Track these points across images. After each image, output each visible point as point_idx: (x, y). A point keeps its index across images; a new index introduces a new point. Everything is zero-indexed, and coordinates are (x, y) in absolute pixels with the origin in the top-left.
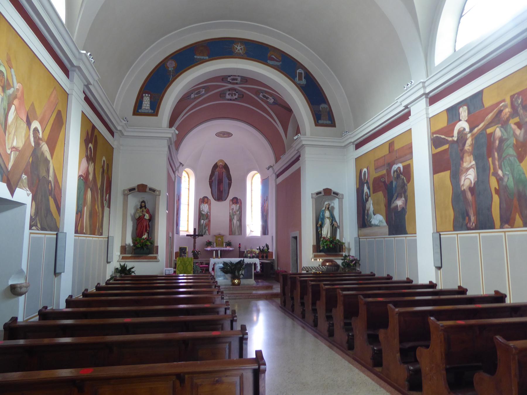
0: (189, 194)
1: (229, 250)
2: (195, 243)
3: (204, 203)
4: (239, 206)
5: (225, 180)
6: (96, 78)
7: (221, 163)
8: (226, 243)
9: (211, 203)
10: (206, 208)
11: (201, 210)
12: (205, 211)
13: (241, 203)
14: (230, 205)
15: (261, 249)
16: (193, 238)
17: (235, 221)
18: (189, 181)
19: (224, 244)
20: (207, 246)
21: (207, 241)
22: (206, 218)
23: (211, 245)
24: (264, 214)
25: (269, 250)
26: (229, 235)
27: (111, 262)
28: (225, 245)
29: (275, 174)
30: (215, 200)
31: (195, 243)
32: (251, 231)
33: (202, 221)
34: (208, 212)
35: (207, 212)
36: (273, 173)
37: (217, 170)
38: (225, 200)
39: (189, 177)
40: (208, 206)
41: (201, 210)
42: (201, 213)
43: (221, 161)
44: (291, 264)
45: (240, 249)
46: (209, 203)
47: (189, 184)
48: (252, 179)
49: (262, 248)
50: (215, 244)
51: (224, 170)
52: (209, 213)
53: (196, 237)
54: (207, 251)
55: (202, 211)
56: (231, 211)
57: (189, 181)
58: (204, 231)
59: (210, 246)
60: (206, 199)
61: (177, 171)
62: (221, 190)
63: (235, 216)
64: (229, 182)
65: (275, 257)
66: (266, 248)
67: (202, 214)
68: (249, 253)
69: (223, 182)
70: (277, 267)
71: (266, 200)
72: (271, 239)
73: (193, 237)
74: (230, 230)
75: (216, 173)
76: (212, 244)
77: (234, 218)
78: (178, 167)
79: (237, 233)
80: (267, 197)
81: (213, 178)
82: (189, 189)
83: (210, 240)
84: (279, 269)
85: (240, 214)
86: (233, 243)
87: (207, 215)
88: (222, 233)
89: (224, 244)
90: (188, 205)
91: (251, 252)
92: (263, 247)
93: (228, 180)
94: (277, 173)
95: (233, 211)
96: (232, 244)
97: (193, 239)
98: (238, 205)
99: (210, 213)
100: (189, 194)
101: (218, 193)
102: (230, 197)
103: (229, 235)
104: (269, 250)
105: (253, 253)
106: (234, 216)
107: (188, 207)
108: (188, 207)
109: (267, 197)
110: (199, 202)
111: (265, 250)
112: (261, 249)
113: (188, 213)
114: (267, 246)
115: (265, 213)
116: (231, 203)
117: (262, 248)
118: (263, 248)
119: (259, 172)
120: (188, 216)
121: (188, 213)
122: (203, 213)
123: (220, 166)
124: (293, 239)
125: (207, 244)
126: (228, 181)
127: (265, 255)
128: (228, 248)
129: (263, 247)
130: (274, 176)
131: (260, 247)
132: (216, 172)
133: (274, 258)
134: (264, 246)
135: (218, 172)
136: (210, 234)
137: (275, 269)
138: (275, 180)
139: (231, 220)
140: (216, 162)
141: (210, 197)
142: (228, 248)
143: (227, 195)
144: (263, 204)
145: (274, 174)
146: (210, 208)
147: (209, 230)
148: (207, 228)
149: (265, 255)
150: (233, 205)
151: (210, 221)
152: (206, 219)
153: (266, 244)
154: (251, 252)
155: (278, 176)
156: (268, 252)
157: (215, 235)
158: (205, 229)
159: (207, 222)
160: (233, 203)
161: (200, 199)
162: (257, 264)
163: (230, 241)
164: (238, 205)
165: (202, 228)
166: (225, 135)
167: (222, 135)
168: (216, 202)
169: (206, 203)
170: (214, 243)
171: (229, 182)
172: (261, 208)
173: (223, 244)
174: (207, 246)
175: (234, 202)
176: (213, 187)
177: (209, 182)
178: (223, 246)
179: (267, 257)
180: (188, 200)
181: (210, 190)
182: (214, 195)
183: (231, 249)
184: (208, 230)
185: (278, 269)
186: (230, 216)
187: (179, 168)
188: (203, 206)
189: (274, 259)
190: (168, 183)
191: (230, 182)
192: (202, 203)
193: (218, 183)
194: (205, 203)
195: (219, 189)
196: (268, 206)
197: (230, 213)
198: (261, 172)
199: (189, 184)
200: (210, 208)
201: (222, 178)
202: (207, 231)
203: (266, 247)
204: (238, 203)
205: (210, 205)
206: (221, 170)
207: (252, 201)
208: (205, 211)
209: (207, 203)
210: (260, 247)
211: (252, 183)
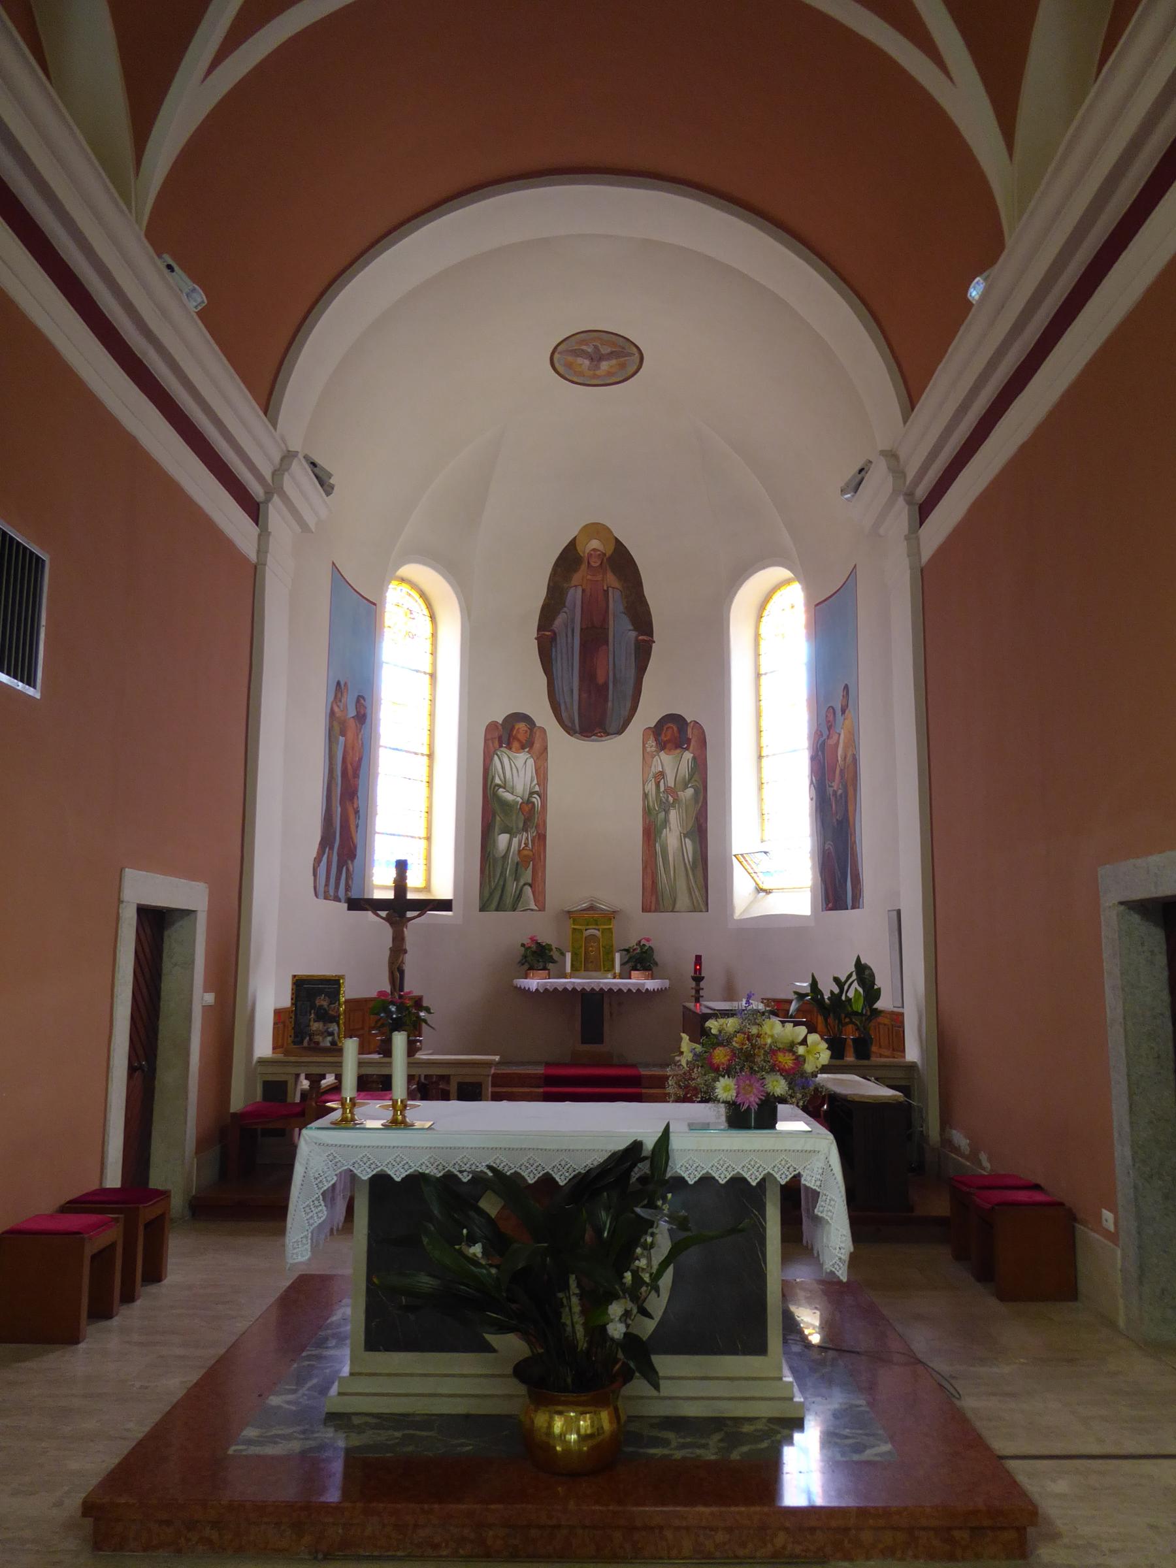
0: (433, 701)
1: (638, 990)
2: (398, 949)
3: (509, 747)
4: (694, 758)
5: (621, 631)
6: (691, 860)
7: (595, 544)
8: (627, 950)
9: (546, 749)
10: (522, 773)
11: (497, 781)
12: (519, 789)
13: (703, 743)
14: (646, 758)
15: (827, 996)
16: (387, 919)
17: (673, 838)
18: (434, 635)
19: (617, 956)
20: (526, 966)
21: (527, 941)
22: (521, 825)
23: (550, 966)
24: (830, 791)
25: (879, 1005)
26: (644, 910)
27: (1116, 902)
28: (622, 964)
29: (909, 495)
30: (570, 730)
31: (398, 949)
32: (759, 890)
33: (503, 839)
34: (531, 793)
35: (526, 796)
36: (895, 492)
37: (577, 578)
38: (620, 732)
39: (433, 617)
40: (531, 762)
41: (497, 781)
42: (495, 795)
43: (596, 529)
44: (1122, 1153)
45: (702, 984)
46: (537, 745)
47: (434, 653)
48: (760, 617)
49: (828, 988)
50: (569, 956)
51: (611, 579)
52: (536, 800)
53: (410, 914)
54: (526, 992)
55: (500, 786)
56: (651, 787)
57: (434, 635)
58: (512, 888)
59: (544, 969)
60: (522, 726)
61: (276, 498)
62: (601, 680)
63: (673, 814)
64: (637, 637)
65: (924, 1051)
66: (854, 990)
67: (505, 805)
68: (729, 1072)
69: (607, 643)
70: (946, 1121)
71: (843, 712)
72: (884, 935)
73: (383, 914)
74: (649, 882)
75: (575, 596)
76: (554, 962)
77: (666, 821)
78: (274, 474)
79: (683, 900)
80: (846, 688)
81: (558, 622)
82: (433, 676)
83: (544, 939)
84: (960, 1139)
85: (696, 802)
86: (663, 954)
87: (527, 808)
88: (607, 899)
89: (617, 956)
90: (431, 756)
91: (749, 1057)
92: (836, 980)
93: (635, 629)
94: (921, 492)
95: (662, 789)
96: (657, 957)
97: (387, 931)
98: (688, 756)
99: (543, 795)
100: (433, 701)
101: (585, 695)
102: (648, 714)
103: (644, 910)
104: (879, 1005)
105: (775, 1068)
106: (667, 812)
107: (431, 767)
108: (431, 767)
109: (846, 688)
110: (486, 740)
111: (849, 1000)
112: (827, 996)
113: (430, 798)
114: (863, 972)
115: (835, 785)
116: (652, 743)
117: (828, 988)
118: (836, 990)
119: (798, 578)
120: (429, 812)
121: (430, 798)
122: (508, 796)
123: (590, 555)
124: (1136, 918)
125: (525, 957)
126: (633, 634)
127: (850, 1034)
128: (639, 981)
129: (836, 980)
130: (902, 514)
131: (814, 984)
132: (572, 591)
133: (912, 1053)
134: (843, 980)
135: (583, 591)
136: (542, 908)
137: (924, 1137)
138: (907, 538)
139: (651, 833)
140: (573, 537)
141: (544, 716)
142: (639, 981)
143: (629, 704)
144: (826, 732)
145: (901, 502)
146: (541, 774)
147: (537, 884)
148: (527, 876)
149: (850, 1034)
150: (662, 754)
151: (541, 838)
152: (525, 829)
153: (858, 959)
154: (749, 1057)
155: (924, 510)
156: (876, 1013)
157: (569, 912)
158: (517, 879)
159: (526, 845)
160: (662, 746)
161: (492, 726)
162: (815, 1195)
163: (648, 940)
164: (688, 756)
165: (503, 873)
166: (605, 366)
167: (587, 362)
168: (572, 740)
169: (523, 747)
170: (563, 954)
171: (640, 638)
172: (813, 759)
173: (613, 961)
174: (526, 966)
175: (669, 741)
176: (558, 667)
177: (540, 639)
178: (613, 967)
179: (863, 1048)
180: (432, 732)
181: (544, 680)
182: (563, 707)
183: (651, 984)
184: (531, 885)
185: (947, 1142)
186: (647, 812)
187: (286, 477)
188: (506, 760)
189: (912, 1067)
190: (374, 673)
191: (643, 641)
192: (501, 746)
193: (583, 645)
194: (516, 745)
195: (588, 677)
196: (853, 742)
197: (645, 796)
198: (807, 575)
199: (434, 653)
200: (541, 774)
201: (605, 619)
202: (528, 890)
203: (855, 984)
204: (689, 741)
205: (541, 757)
206: (599, 578)
207: (759, 732)
208: (519, 789)
209: (526, 745)
210: (814, 984)
211: (757, 637)
